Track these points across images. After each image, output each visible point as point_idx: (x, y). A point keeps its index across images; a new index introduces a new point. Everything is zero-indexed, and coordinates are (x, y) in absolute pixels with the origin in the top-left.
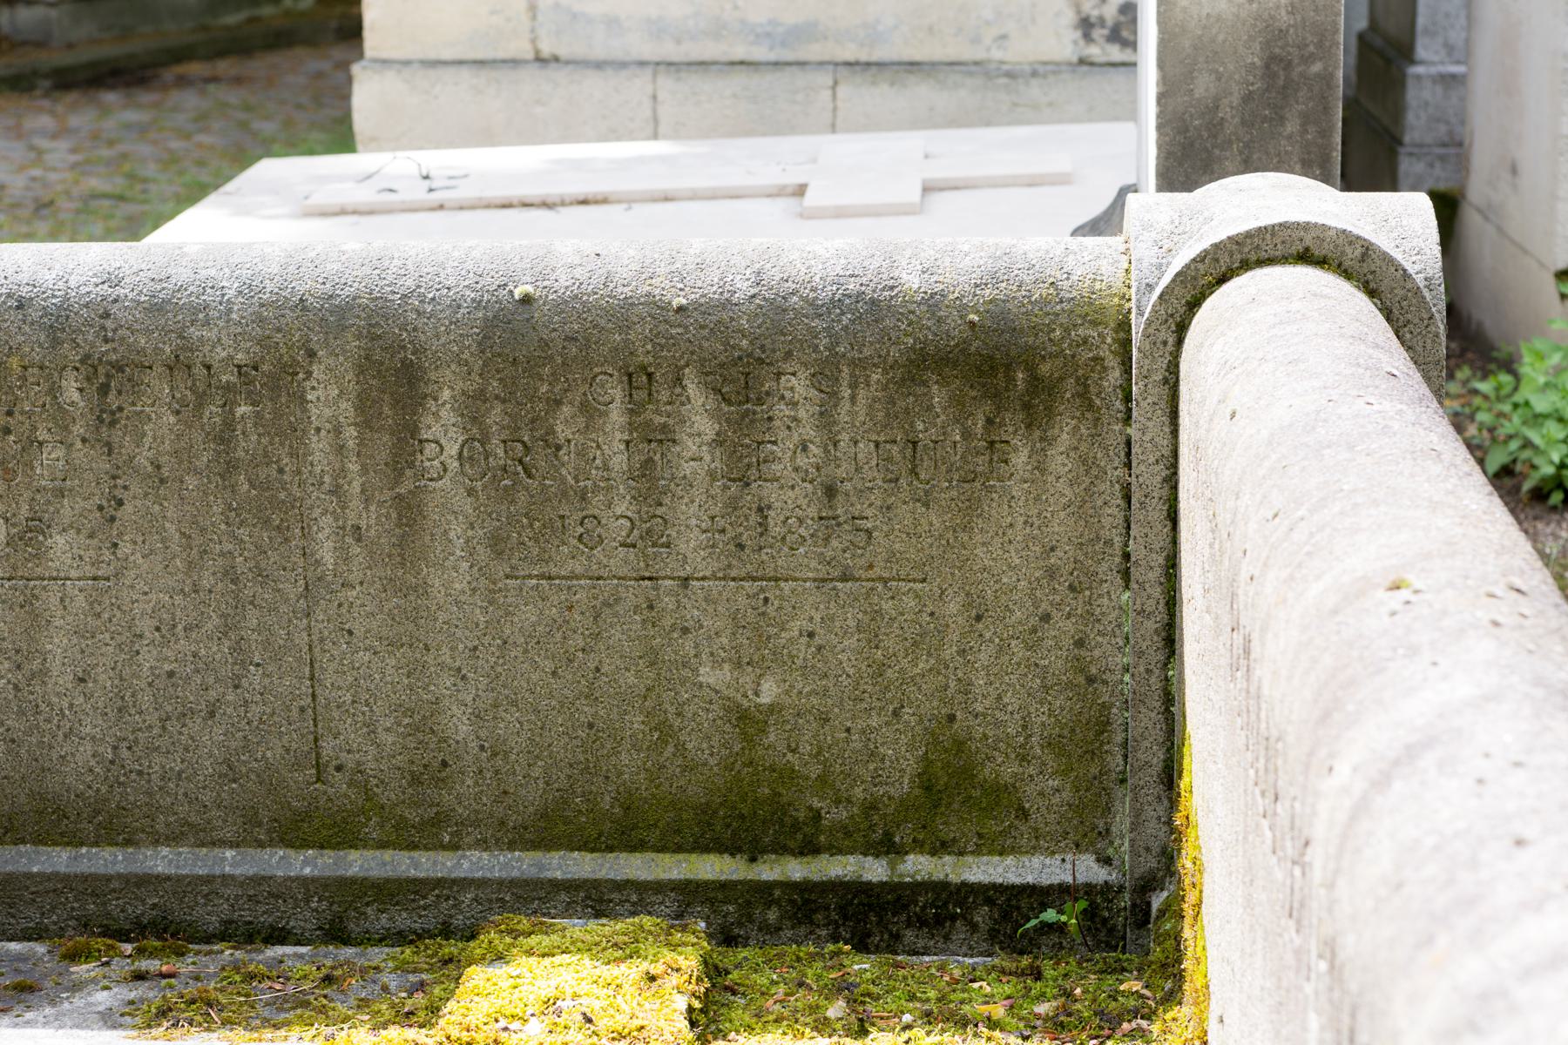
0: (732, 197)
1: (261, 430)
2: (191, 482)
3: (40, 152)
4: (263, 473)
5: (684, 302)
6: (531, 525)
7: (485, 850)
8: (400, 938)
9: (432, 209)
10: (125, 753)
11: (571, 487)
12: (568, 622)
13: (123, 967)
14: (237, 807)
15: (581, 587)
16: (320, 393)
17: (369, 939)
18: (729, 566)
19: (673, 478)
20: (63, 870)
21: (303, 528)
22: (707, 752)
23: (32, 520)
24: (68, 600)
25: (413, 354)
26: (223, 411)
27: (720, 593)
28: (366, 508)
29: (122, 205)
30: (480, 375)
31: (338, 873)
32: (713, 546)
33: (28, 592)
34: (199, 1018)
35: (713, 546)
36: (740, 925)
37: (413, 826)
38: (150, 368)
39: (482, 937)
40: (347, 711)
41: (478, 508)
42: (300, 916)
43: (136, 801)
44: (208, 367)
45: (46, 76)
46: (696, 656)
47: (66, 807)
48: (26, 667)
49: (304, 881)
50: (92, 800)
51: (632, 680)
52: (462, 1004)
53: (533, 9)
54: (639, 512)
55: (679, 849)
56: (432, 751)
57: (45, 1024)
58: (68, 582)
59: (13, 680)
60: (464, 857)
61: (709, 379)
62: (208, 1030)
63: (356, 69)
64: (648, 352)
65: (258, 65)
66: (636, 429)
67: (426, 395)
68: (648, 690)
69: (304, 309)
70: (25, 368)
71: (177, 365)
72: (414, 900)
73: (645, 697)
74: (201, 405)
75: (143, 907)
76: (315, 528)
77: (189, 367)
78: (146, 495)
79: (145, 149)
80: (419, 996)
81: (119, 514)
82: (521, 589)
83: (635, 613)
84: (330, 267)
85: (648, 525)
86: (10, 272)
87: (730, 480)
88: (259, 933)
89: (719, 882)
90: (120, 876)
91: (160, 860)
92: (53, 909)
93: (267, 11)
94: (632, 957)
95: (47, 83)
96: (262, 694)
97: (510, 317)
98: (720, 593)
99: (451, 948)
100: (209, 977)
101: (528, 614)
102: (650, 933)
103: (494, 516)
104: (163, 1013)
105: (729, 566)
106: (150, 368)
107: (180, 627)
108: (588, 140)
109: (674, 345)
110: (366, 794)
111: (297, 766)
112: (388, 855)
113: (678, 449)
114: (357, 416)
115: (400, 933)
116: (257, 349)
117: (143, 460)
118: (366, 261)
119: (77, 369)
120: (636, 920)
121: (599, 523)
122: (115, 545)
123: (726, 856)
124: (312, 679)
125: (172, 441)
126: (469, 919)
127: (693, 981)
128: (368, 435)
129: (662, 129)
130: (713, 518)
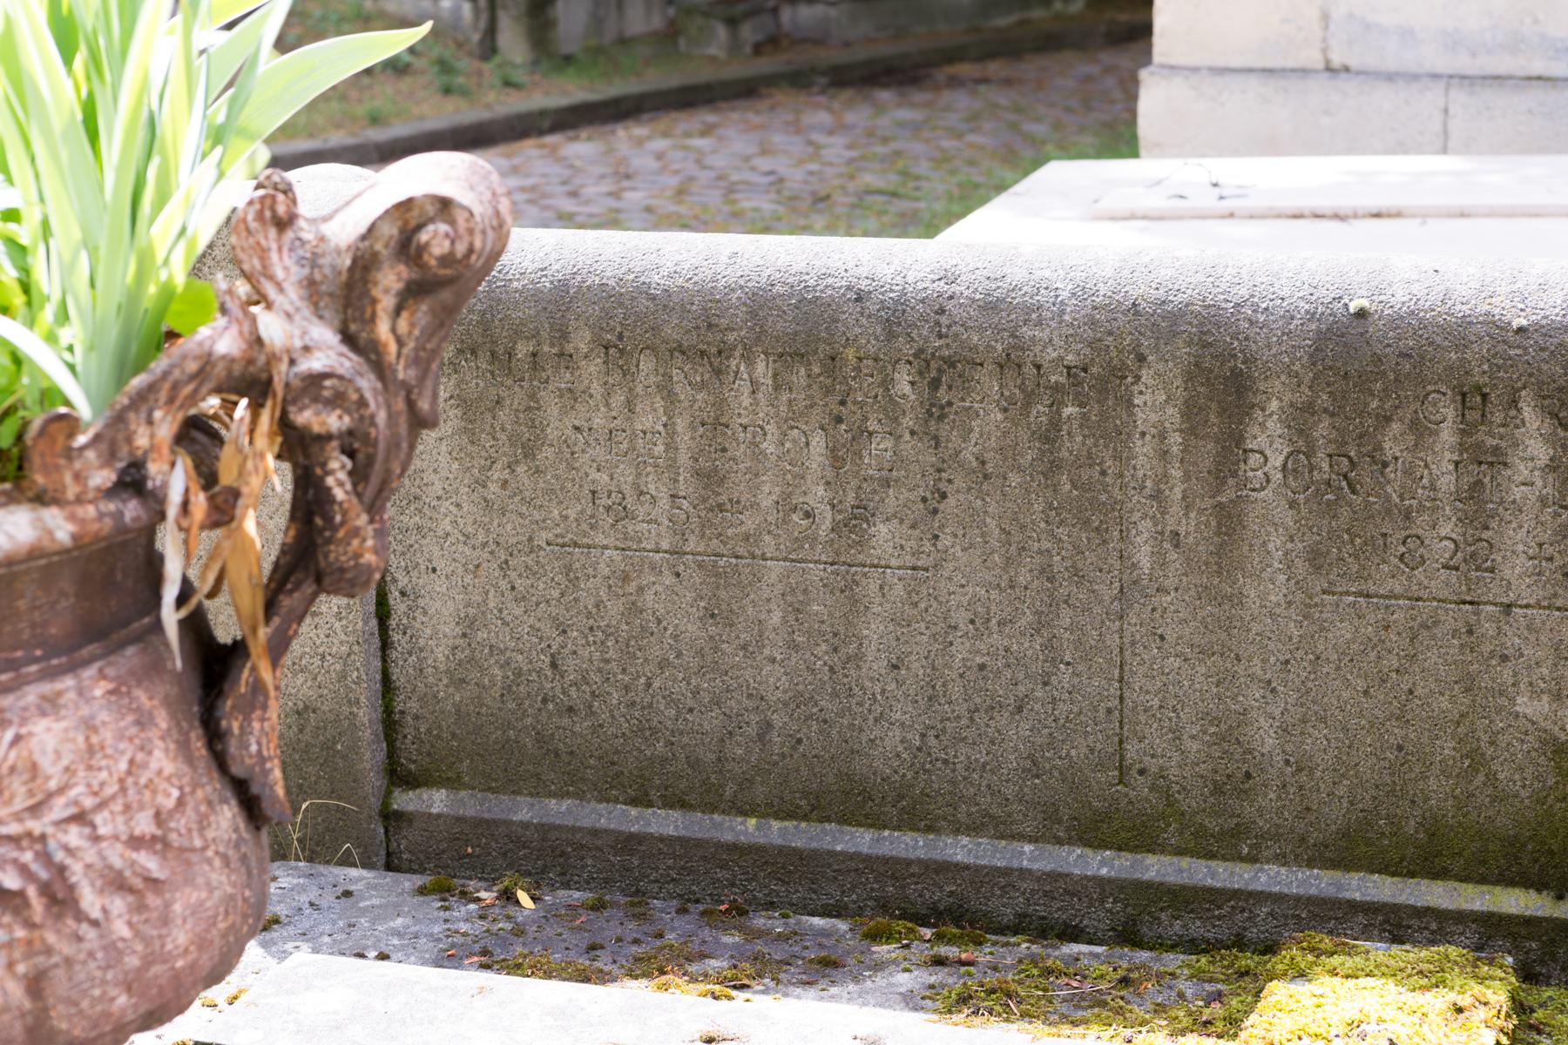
0: (1531, 215)
1: (1086, 432)
2: (1015, 479)
3: (818, 147)
4: (1085, 474)
5: (1524, 322)
6: (1352, 542)
7: (1283, 865)
8: (1193, 946)
9: (1223, 217)
10: (932, 742)
11: (1396, 505)
12: (1383, 642)
13: (922, 951)
14: (1039, 803)
15: (1400, 607)
16: (1147, 397)
17: (1161, 945)
18: (1555, 595)
19: (1502, 502)
20: (865, 850)
21: (1121, 531)
22: (1519, 783)
23: (858, 507)
24: (887, 588)
25: (1243, 363)
26: (1050, 411)
27: (1544, 623)
28: (1186, 515)
29: (895, 201)
30: (1310, 387)
31: (1135, 876)
32: (1539, 574)
33: (849, 577)
34: (998, 1008)
35: (1539, 574)
36: (1542, 962)
37: (1212, 836)
38: (982, 365)
39: (1284, 953)
40: (1154, 715)
41: (1299, 521)
42: (1094, 916)
43: (940, 789)
44: (1038, 367)
45: (823, 73)
46: (1514, 685)
47: (872, 789)
48: (843, 651)
49: (1100, 881)
50: (897, 785)
51: (1445, 705)
52: (1265, 1018)
53: (1325, 18)
54: (1464, 535)
55: (1483, 880)
56: (1237, 761)
57: (849, 1000)
58: (888, 571)
59: (829, 662)
60: (1262, 870)
61: (1546, 402)
62: (1007, 1020)
63: (1144, 74)
64: (1484, 372)
65: (1029, 67)
66: (1466, 450)
67: (1253, 406)
68: (1462, 716)
69: (1137, 313)
70: (860, 359)
71: (1008, 364)
72: (1209, 910)
73: (1458, 723)
74: (1029, 403)
75: (940, 895)
76: (1134, 532)
77: (1019, 366)
78: (970, 489)
79: (917, 147)
80: (1216, 1005)
81: (941, 507)
82: (1338, 606)
83: (1453, 637)
84: (1163, 272)
85: (1473, 548)
86: (850, 265)
87: (1562, 507)
88: (1052, 929)
89: (1524, 917)
90: (920, 861)
91: (960, 849)
92: (854, 887)
93: (1037, 13)
94: (1437, 987)
95: (824, 80)
96: (1070, 693)
97: (1344, 330)
98: (1544, 623)
99: (1247, 960)
100: (1007, 968)
101: (1344, 631)
102: (1456, 963)
103: (1315, 530)
104: (964, 999)
105: (1555, 595)
106: (982, 365)
107: (994, 621)
108: (1375, 152)
109: (1512, 366)
110: (1167, 799)
111: (1101, 766)
112: (1185, 862)
113: (1509, 472)
114: (1183, 422)
115: (1193, 941)
116: (1088, 351)
117: (968, 455)
118: (1200, 269)
119: (910, 363)
120: (1441, 949)
121: (1422, 543)
122: (936, 537)
123: (1531, 891)
124: (1121, 680)
125: (998, 438)
126: (1263, 933)
127: (1502, 1016)
128: (1193, 442)
129: (1451, 144)
130: (1540, 545)
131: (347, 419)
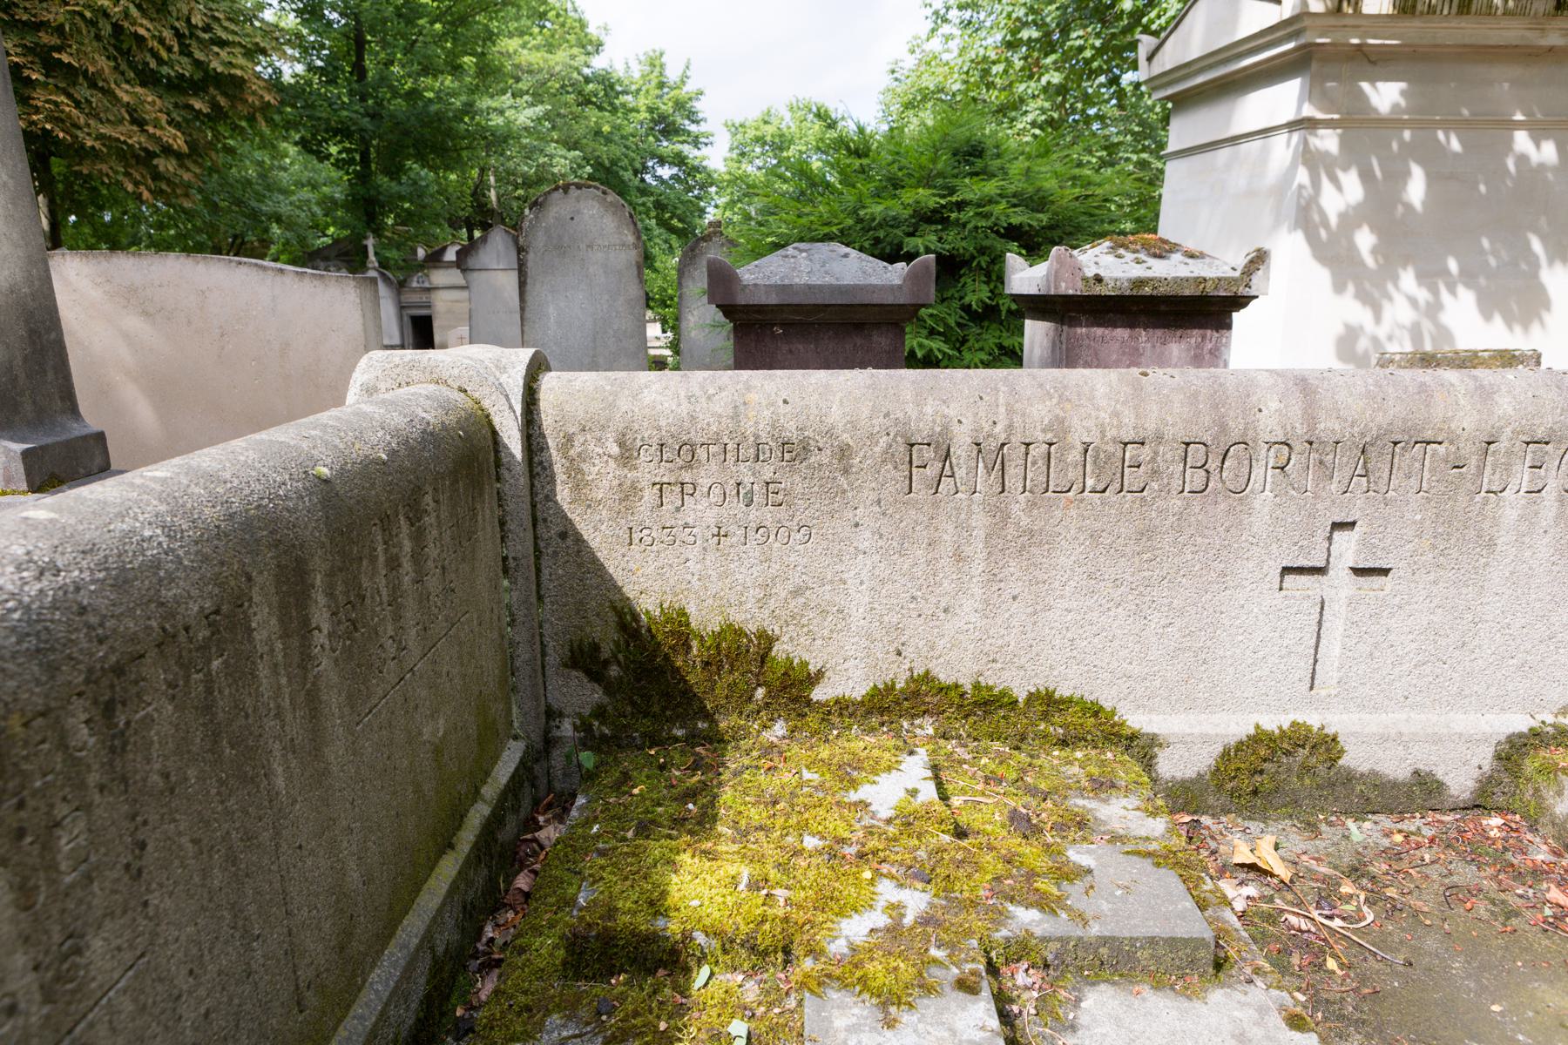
60: (371, 983)
71: (166, 640)
131: (1484, 822)
